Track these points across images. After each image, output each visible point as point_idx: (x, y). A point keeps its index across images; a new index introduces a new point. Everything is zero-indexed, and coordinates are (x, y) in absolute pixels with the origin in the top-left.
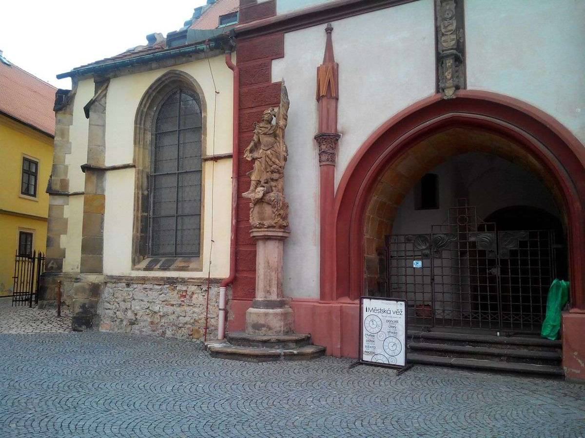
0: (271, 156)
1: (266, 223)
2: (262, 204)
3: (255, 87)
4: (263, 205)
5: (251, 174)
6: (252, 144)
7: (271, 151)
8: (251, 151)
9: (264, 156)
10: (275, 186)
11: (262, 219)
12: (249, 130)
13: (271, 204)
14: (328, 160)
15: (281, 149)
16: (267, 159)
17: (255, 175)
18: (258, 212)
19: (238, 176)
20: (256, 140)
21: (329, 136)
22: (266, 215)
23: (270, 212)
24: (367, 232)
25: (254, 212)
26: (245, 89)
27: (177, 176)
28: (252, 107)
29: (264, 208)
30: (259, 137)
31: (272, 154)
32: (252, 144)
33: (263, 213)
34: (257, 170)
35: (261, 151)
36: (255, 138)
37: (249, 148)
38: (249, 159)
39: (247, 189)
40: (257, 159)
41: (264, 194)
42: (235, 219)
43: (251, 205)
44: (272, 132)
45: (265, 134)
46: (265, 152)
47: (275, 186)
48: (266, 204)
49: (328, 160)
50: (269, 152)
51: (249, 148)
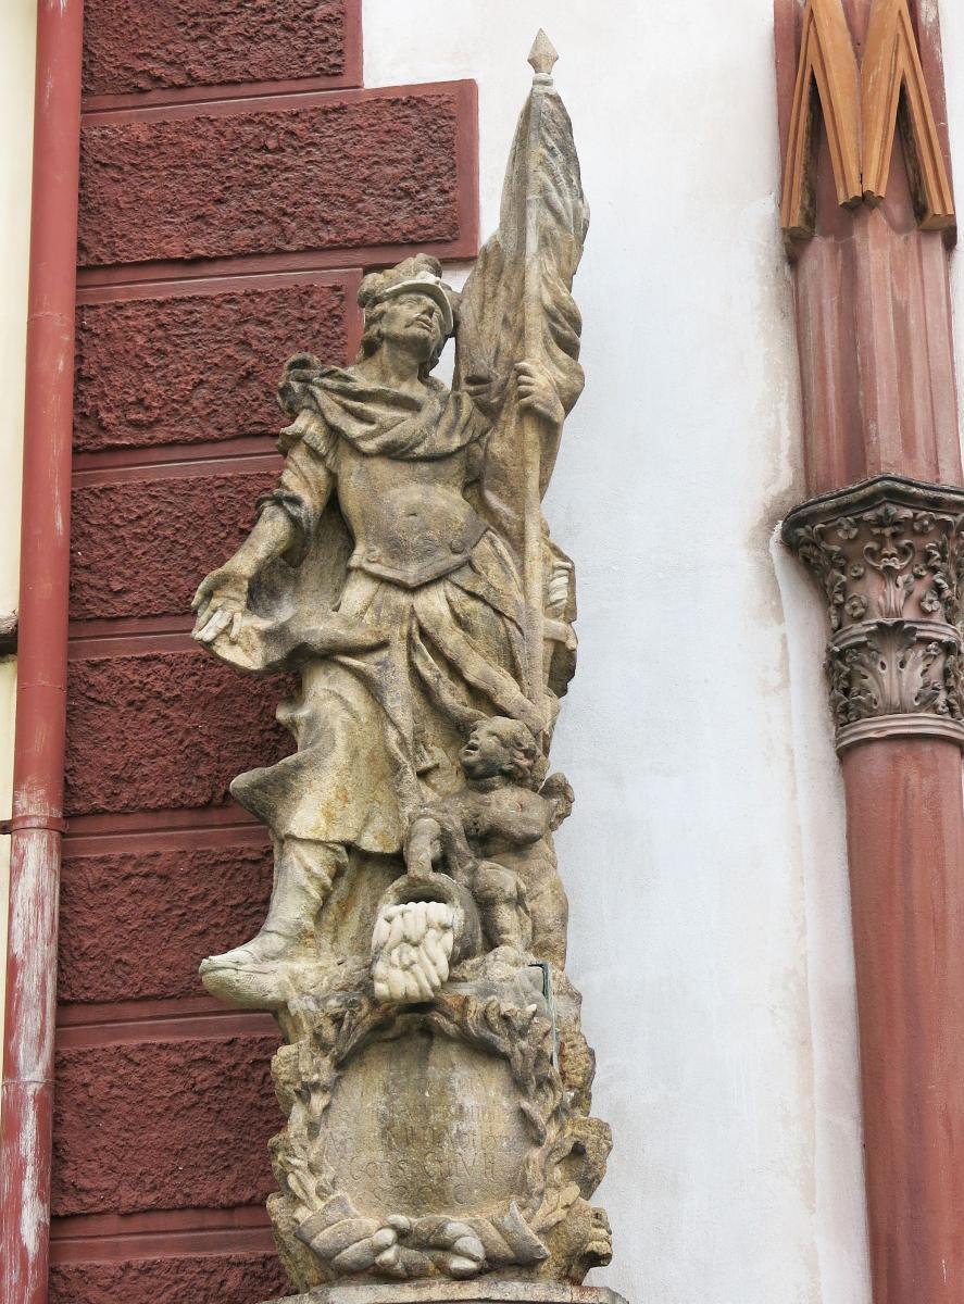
0: (452, 639)
1: (468, 1232)
2: (424, 1059)
3: (228, 106)
4: (434, 1072)
5: (282, 787)
6: (271, 531)
7: (457, 596)
8: (261, 592)
9: (397, 634)
10: (518, 901)
11: (423, 1191)
12: (161, 434)
13: (505, 1058)
14: (927, 702)
15: (536, 588)
16: (430, 668)
17: (330, 794)
18: (387, 1129)
19: (70, 816)
20: (307, 500)
21: (935, 504)
22: (469, 1158)
23: (504, 1124)
24: (563, 1297)
25: (338, 1129)
26: (134, 123)
27: (814, 484)
28: (197, 261)
29: (444, 1089)
30: (333, 477)
31: (461, 622)
32: (271, 531)
33: (438, 1138)
34: (339, 756)
35: (357, 593)
36: (301, 480)
37: (244, 562)
38: (247, 657)
39: (247, 919)
40: (331, 655)
41: (455, 961)
42: (40, 1193)
43: (293, 1060)
44: (457, 442)
45: (395, 452)
46: (403, 600)
47: (518, 901)
48: (453, 1052)
49: (927, 702)
50: (434, 604)
51: (244, 562)
